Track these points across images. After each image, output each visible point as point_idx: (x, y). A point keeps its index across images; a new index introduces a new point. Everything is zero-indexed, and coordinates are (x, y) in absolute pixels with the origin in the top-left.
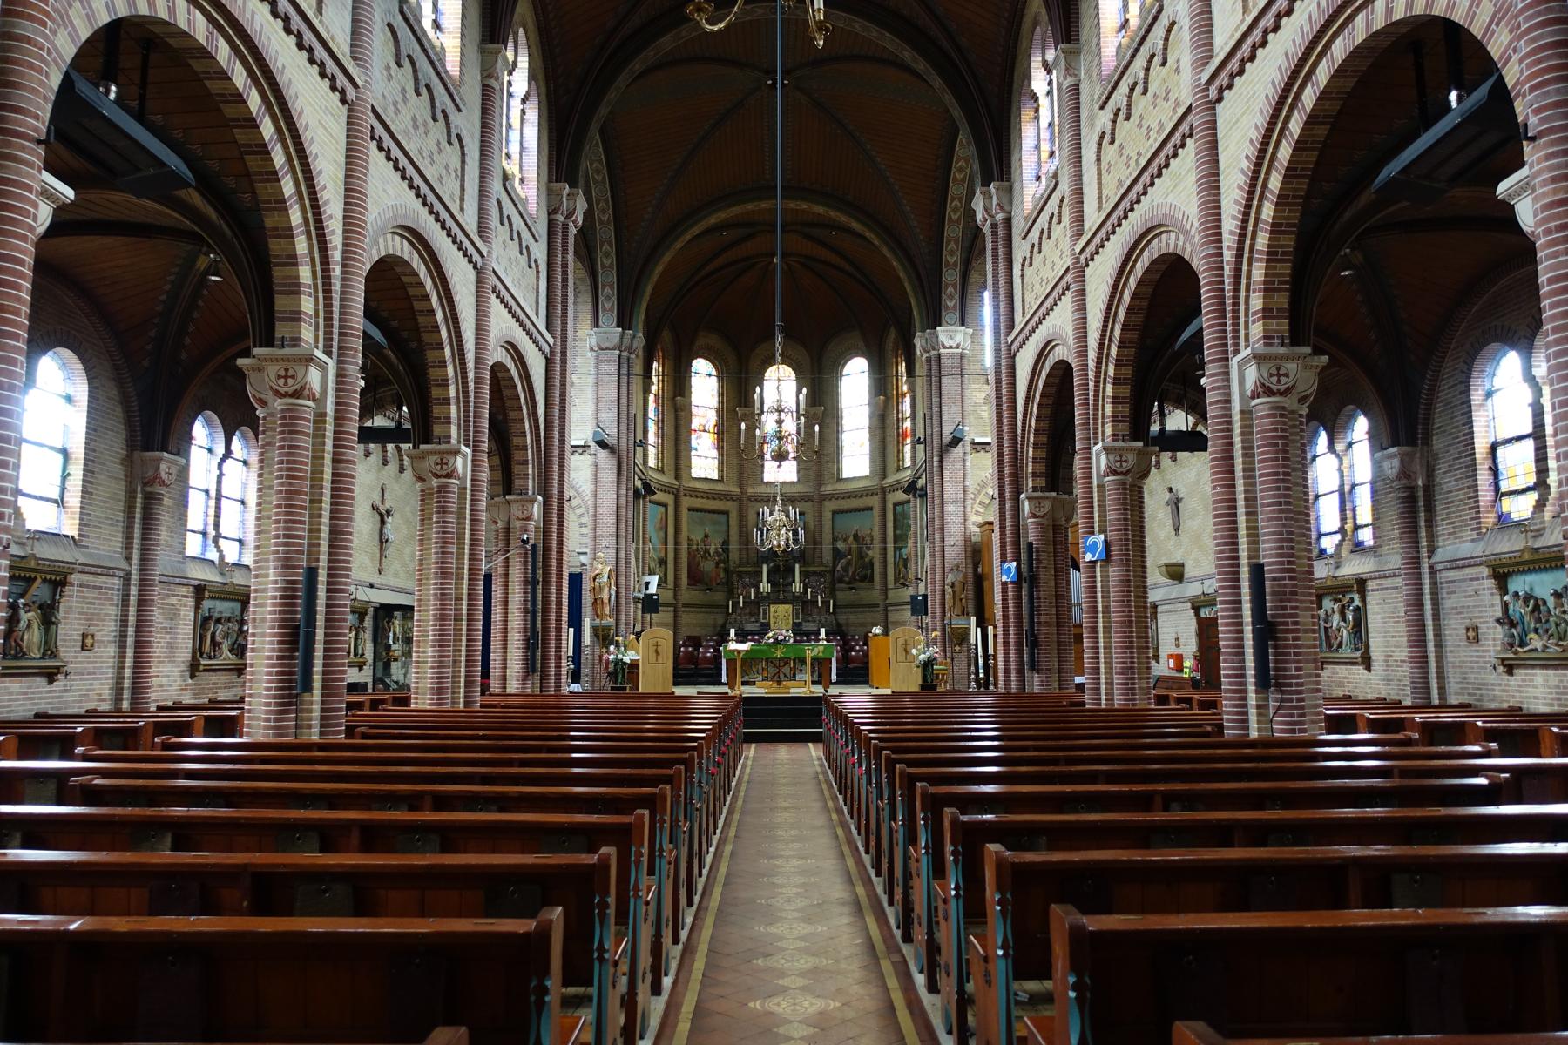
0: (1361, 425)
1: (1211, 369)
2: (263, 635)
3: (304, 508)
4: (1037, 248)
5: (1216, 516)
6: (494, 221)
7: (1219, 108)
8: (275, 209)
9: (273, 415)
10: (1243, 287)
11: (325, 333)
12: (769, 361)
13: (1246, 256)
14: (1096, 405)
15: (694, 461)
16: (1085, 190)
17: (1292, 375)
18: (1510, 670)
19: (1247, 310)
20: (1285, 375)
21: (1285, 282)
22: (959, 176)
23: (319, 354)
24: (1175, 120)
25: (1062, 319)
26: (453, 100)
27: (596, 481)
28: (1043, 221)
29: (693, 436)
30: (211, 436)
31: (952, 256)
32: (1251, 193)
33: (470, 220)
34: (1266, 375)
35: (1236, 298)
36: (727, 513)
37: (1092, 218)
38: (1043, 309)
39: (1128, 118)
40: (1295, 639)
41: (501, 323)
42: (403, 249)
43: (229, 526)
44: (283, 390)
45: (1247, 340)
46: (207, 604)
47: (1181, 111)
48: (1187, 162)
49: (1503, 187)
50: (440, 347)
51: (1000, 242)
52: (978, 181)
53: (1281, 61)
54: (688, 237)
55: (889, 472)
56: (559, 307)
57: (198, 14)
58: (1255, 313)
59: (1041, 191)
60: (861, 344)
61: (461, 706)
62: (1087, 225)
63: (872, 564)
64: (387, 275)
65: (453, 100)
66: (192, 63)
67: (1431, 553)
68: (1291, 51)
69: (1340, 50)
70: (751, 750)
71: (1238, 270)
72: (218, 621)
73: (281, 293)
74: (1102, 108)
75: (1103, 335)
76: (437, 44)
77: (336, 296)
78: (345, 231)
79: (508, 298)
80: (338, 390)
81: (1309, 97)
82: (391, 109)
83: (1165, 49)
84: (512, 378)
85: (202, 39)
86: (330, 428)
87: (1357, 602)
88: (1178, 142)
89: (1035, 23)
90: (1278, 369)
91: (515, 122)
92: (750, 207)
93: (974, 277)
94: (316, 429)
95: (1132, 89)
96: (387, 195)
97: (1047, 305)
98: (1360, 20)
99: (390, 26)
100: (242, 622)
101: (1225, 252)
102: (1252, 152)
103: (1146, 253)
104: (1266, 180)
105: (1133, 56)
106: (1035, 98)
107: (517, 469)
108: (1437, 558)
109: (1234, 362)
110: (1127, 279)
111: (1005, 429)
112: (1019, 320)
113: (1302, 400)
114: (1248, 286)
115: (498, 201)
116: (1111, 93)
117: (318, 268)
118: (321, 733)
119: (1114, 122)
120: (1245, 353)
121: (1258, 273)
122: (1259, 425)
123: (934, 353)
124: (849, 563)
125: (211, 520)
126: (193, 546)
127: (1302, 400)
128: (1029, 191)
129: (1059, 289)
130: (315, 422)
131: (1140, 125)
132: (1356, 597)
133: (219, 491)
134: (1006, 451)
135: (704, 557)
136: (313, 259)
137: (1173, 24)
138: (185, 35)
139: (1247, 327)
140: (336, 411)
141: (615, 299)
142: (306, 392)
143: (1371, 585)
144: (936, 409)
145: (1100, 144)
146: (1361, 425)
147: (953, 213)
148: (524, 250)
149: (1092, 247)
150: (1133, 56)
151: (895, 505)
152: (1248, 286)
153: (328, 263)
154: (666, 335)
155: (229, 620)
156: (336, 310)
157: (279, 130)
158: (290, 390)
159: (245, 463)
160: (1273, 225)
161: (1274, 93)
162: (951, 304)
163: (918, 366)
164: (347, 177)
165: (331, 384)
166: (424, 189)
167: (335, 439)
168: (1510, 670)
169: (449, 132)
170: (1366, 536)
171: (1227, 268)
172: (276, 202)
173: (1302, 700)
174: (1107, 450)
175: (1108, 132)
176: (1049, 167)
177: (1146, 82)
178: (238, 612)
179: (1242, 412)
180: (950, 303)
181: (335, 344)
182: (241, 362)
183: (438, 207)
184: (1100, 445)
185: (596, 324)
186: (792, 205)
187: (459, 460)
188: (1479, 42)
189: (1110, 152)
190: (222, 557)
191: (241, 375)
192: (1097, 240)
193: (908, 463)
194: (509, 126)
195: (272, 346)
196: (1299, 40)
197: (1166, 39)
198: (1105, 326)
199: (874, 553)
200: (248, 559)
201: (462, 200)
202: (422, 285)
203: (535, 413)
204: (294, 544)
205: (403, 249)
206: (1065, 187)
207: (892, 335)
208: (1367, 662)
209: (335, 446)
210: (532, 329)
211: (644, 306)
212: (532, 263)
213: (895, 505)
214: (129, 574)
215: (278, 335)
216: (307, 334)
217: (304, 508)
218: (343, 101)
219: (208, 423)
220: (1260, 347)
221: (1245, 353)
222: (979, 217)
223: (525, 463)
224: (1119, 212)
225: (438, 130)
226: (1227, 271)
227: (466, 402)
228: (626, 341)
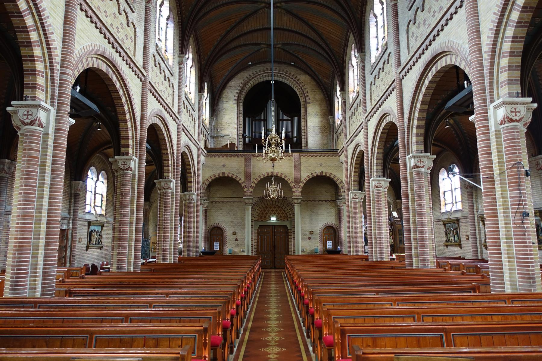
4: (377, 76)
18: (447, 246)
20: (519, 112)
21: (518, 66)
28: (355, 105)
33: (175, 110)
38: (378, 105)
43: (98, 203)
61: (38, 295)
69: (434, 71)
74: (410, 10)
76: (166, 57)
82: (116, 30)
88: (418, 57)
96: (153, 105)
98: (434, 68)
106: (376, 17)
109: (408, 157)
125: (93, 201)
126: (88, 208)
127: (428, 169)
131: (382, 81)
133: (95, 192)
137: (390, 53)
145: (371, 85)
148: (191, 115)
159: (103, 182)
168: (447, 246)
172: (23, 28)
179: (410, 173)
183: (166, 107)
187: (172, 183)
190: (96, 213)
194: (186, 76)
195: (22, 100)
204: (29, 197)
206: (361, 97)
221: (411, 155)
225: (166, 83)
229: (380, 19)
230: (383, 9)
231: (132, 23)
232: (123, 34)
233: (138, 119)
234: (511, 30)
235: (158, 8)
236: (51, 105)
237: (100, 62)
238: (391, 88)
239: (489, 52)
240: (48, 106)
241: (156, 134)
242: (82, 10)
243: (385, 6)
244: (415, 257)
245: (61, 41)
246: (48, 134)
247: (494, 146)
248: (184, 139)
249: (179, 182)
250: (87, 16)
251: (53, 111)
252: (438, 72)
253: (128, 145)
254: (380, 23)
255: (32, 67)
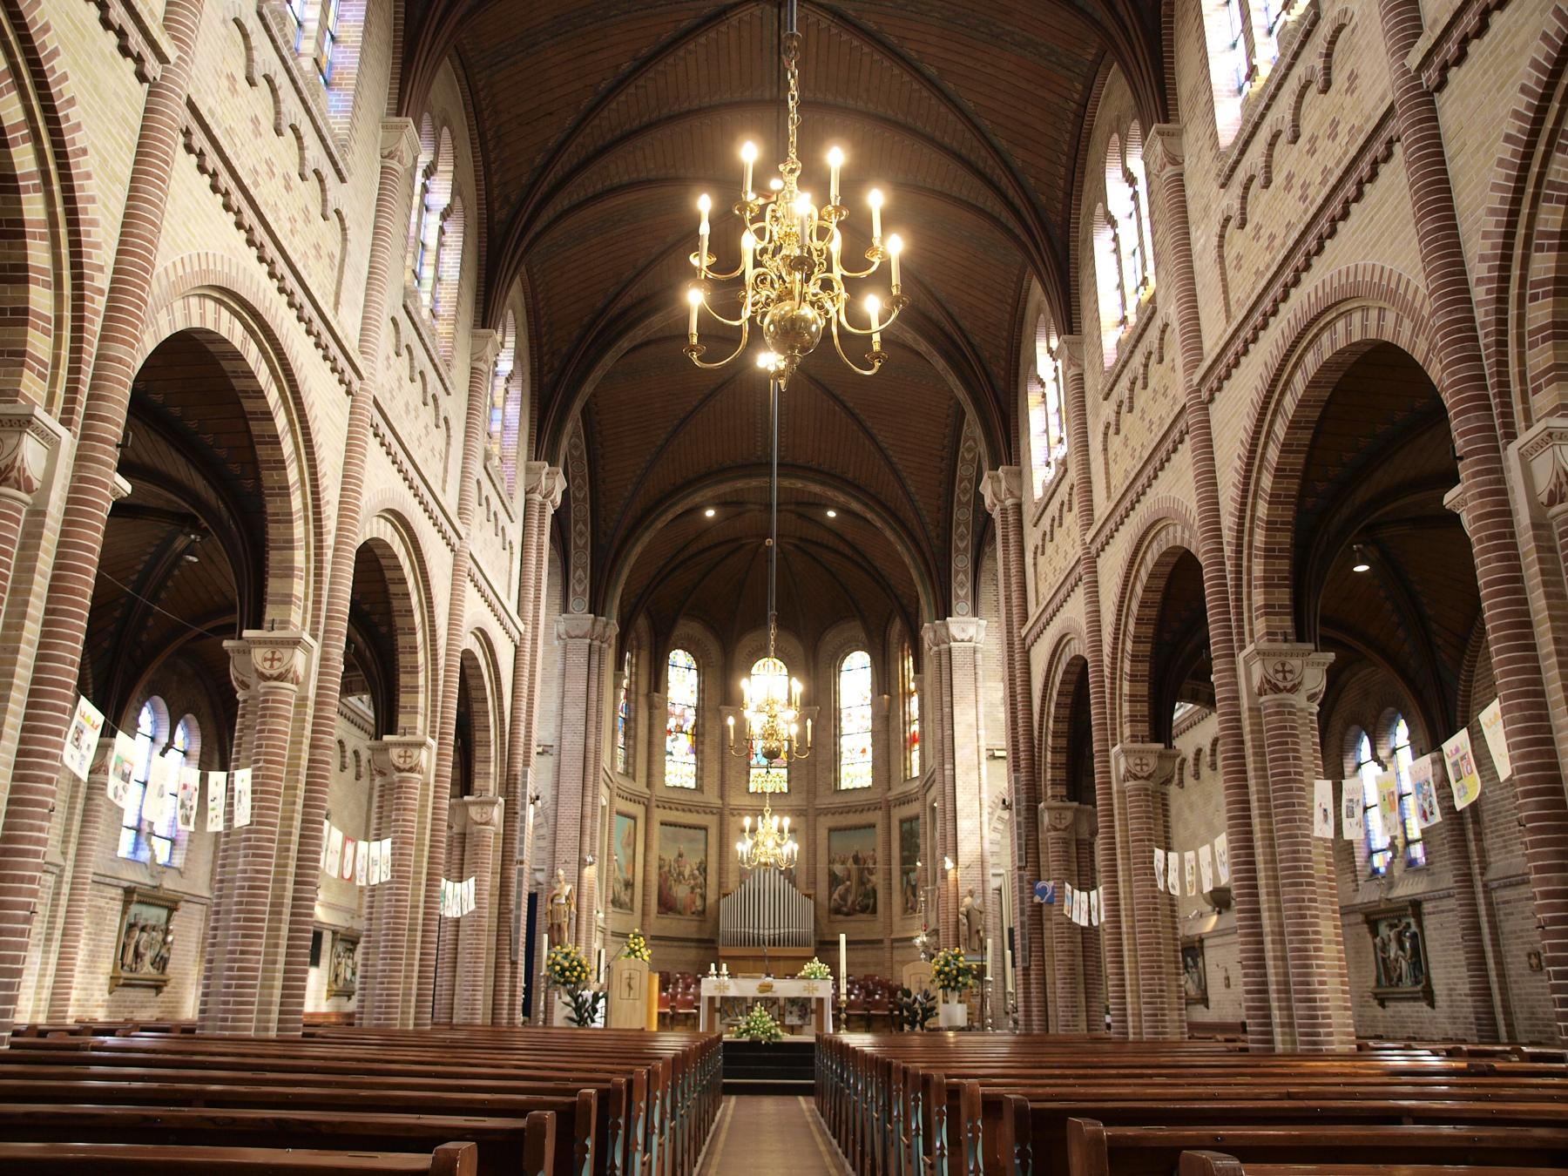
0: (1402, 731)
1: (1217, 665)
2: (227, 928)
3: (278, 794)
4: (1048, 536)
5: (1230, 818)
6: (473, 503)
7: (1212, 408)
8: (278, 495)
9: (254, 698)
10: (1245, 583)
11: (313, 616)
12: (762, 652)
13: (1245, 552)
14: (1113, 704)
15: (669, 767)
16: (1094, 479)
17: (1297, 672)
19: (1250, 606)
22: (968, 456)
23: (307, 637)
24: (1172, 417)
25: (1075, 611)
26: (444, 385)
27: (557, 785)
28: (1054, 508)
29: (669, 738)
30: (155, 723)
31: (962, 542)
32: (1245, 491)
33: (450, 502)
34: (1271, 671)
35: (1238, 593)
36: (705, 829)
37: (1102, 507)
39: (1131, 410)
40: (1316, 949)
41: (475, 611)
42: (386, 532)
44: (268, 672)
45: (1252, 635)
46: (134, 909)
47: (1177, 409)
48: (1185, 458)
49: (1448, 497)
50: (413, 631)
51: (1011, 528)
52: (985, 465)
53: (1262, 369)
54: (670, 516)
55: (893, 783)
56: (532, 591)
57: (237, 323)
58: (1257, 609)
59: (1050, 477)
60: (862, 636)
62: (1097, 514)
63: (874, 891)
64: (372, 560)
65: (444, 385)
66: (223, 363)
67: (1484, 869)
68: (1270, 362)
69: (1311, 363)
70: (730, 1104)
71: (1238, 565)
72: (143, 929)
73: (275, 576)
74: (1105, 399)
75: (1117, 629)
77: (326, 580)
78: (340, 516)
79: (484, 586)
80: (320, 674)
81: (1289, 404)
82: (388, 395)
83: (1161, 348)
84: (479, 667)
85: (237, 345)
86: (310, 711)
87: (1414, 928)
89: (1039, 311)
90: (1283, 665)
91: (499, 401)
92: (740, 484)
93: (986, 564)
94: (297, 713)
95: (1133, 383)
97: (1061, 596)
99: (393, 319)
100: (167, 932)
101: (1226, 548)
102: (1243, 452)
103: (1155, 544)
104: (1258, 480)
105: (1132, 352)
106: (1112, 222)
107: (478, 767)
108: (1490, 875)
109: (1241, 657)
110: (1138, 571)
111: (1021, 730)
112: (1033, 611)
113: (1311, 698)
114: (1249, 581)
115: (478, 482)
116: (1114, 385)
117: (312, 552)
118: (279, 1029)
119: (1118, 413)
120: (1250, 648)
121: (1258, 569)
122: (1268, 723)
123: (944, 646)
124: (848, 890)
127: (1311, 698)
128: (1040, 476)
129: (1072, 580)
130: (297, 706)
132: (1412, 921)
134: (1022, 755)
135: (677, 881)
136: (307, 544)
137: (1166, 325)
138: (225, 341)
139: (1251, 623)
140: (318, 695)
141: (587, 582)
142: (291, 675)
143: (1427, 907)
144: (947, 710)
145: (1106, 434)
146: (1402, 731)
147: (962, 495)
149: (1102, 538)
150: (1132, 352)
151: (902, 822)
152: (1249, 581)
153: (321, 548)
154: (642, 623)
155: (154, 928)
156: (325, 593)
157: (291, 422)
158: (275, 673)
159: (185, 753)
160: (1268, 522)
161: (1258, 399)
162: (962, 593)
163: (926, 660)
164: (346, 463)
165: (315, 668)
166: (412, 473)
167: (314, 724)
169: (437, 415)
170: (1417, 851)
171: (1228, 563)
173: (1329, 1017)
174: (1126, 752)
175: (1113, 423)
176: (1060, 452)
177: (1145, 378)
178: (163, 920)
179: (1250, 709)
180: (961, 591)
181: (322, 627)
182: (226, 644)
183: (423, 490)
184: (1117, 747)
185: (565, 609)
186: (786, 483)
188: (1421, 368)
189: (1115, 442)
190: (154, 857)
191: (225, 657)
192: (1107, 531)
193: (916, 773)
194: (493, 405)
196: (1275, 353)
197: (1162, 339)
198: (1119, 619)
199: (877, 880)
200: (178, 861)
201: (444, 481)
202: (400, 568)
203: (501, 706)
205: (386, 532)
206: (1073, 475)
207: (897, 627)
208: (1429, 997)
209: (313, 732)
210: (504, 615)
211: (620, 590)
212: (507, 546)
213: (902, 822)
214: (63, 870)
215: (268, 617)
216: (296, 616)
217: (278, 794)
218: (349, 393)
219: (154, 710)
220: (1264, 645)
222: (988, 502)
223: (487, 760)
224: (1127, 503)
226: (1229, 567)
227: (435, 691)
228: (599, 628)
229: (1127, 230)
230: (1135, 196)
231: (338, 212)
232: (306, 240)
233: (330, 512)
234: (1554, 211)
235: (419, 179)
236: (62, 422)
237: (225, 313)
238: (1175, 434)
239: (1490, 280)
240: (52, 422)
241: (383, 581)
242: (189, 148)
243: (1142, 187)
244: (1283, 1025)
245: (114, 245)
246: (43, 514)
247: (1548, 656)
248: (475, 611)
249: (450, 750)
250: (202, 169)
251: (68, 441)
252: (1325, 368)
253: (290, 595)
254: (1129, 240)
255: (14, 300)
